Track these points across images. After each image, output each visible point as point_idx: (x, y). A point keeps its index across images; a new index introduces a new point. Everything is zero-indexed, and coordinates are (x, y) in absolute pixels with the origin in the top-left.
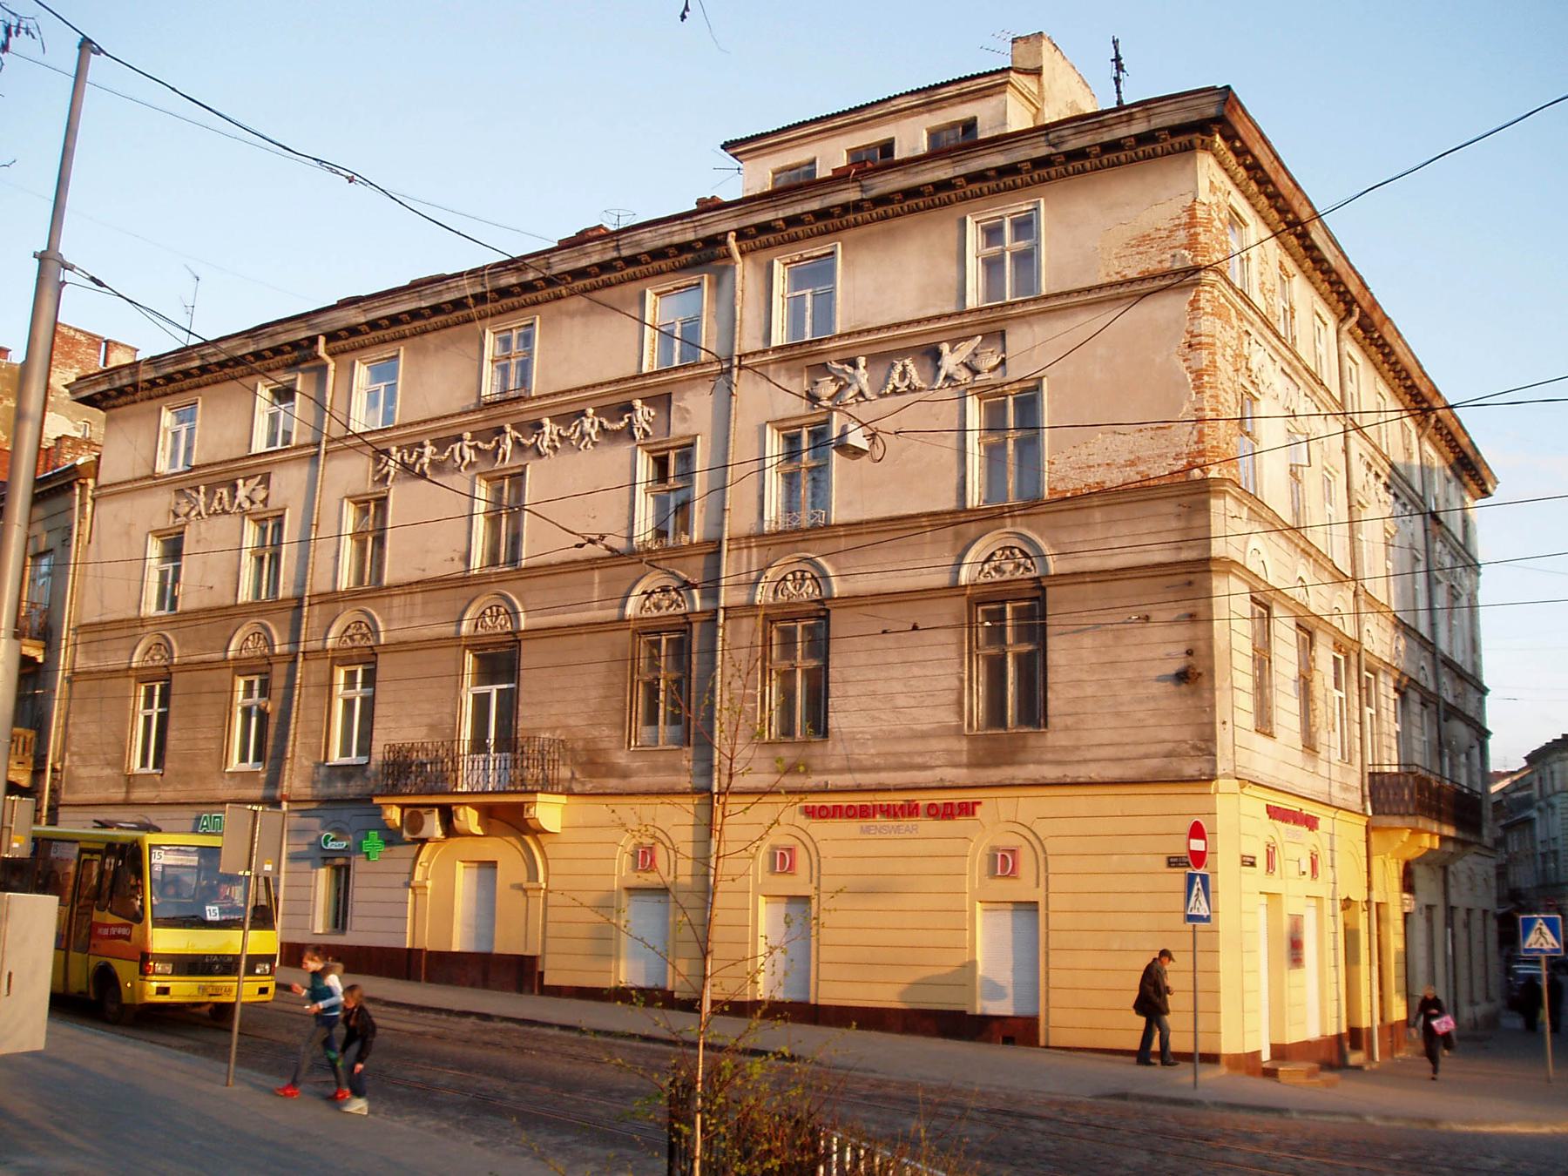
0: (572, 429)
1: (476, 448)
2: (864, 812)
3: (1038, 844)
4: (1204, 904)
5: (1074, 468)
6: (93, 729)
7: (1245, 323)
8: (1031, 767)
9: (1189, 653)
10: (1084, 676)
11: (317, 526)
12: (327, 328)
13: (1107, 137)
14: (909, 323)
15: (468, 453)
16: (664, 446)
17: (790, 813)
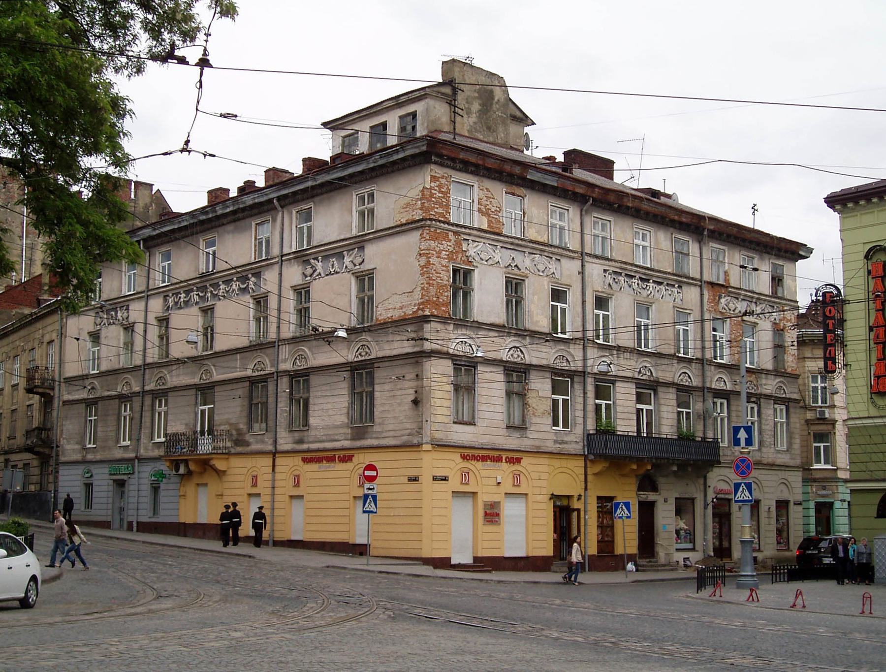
4: (374, 506)
6: (71, 427)
7: (462, 236)
8: (369, 440)
17: (297, 460)
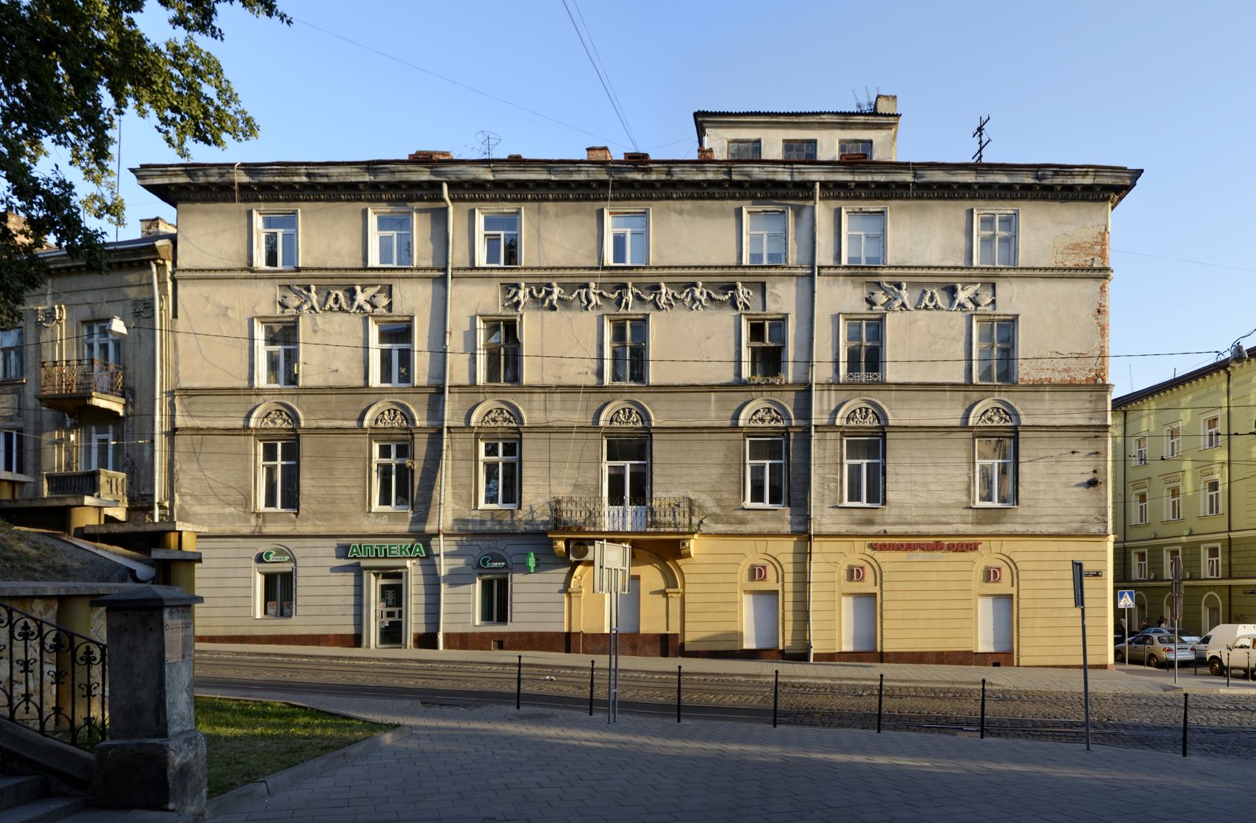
0: (684, 294)
1: (601, 295)
2: (910, 547)
3: (1013, 565)
5: (1033, 369)
8: (1009, 525)
9: (1095, 471)
10: (1040, 480)
11: (450, 333)
12: (453, 178)
13: (1069, 181)
14: (936, 268)
15: (594, 298)
16: (762, 317)
